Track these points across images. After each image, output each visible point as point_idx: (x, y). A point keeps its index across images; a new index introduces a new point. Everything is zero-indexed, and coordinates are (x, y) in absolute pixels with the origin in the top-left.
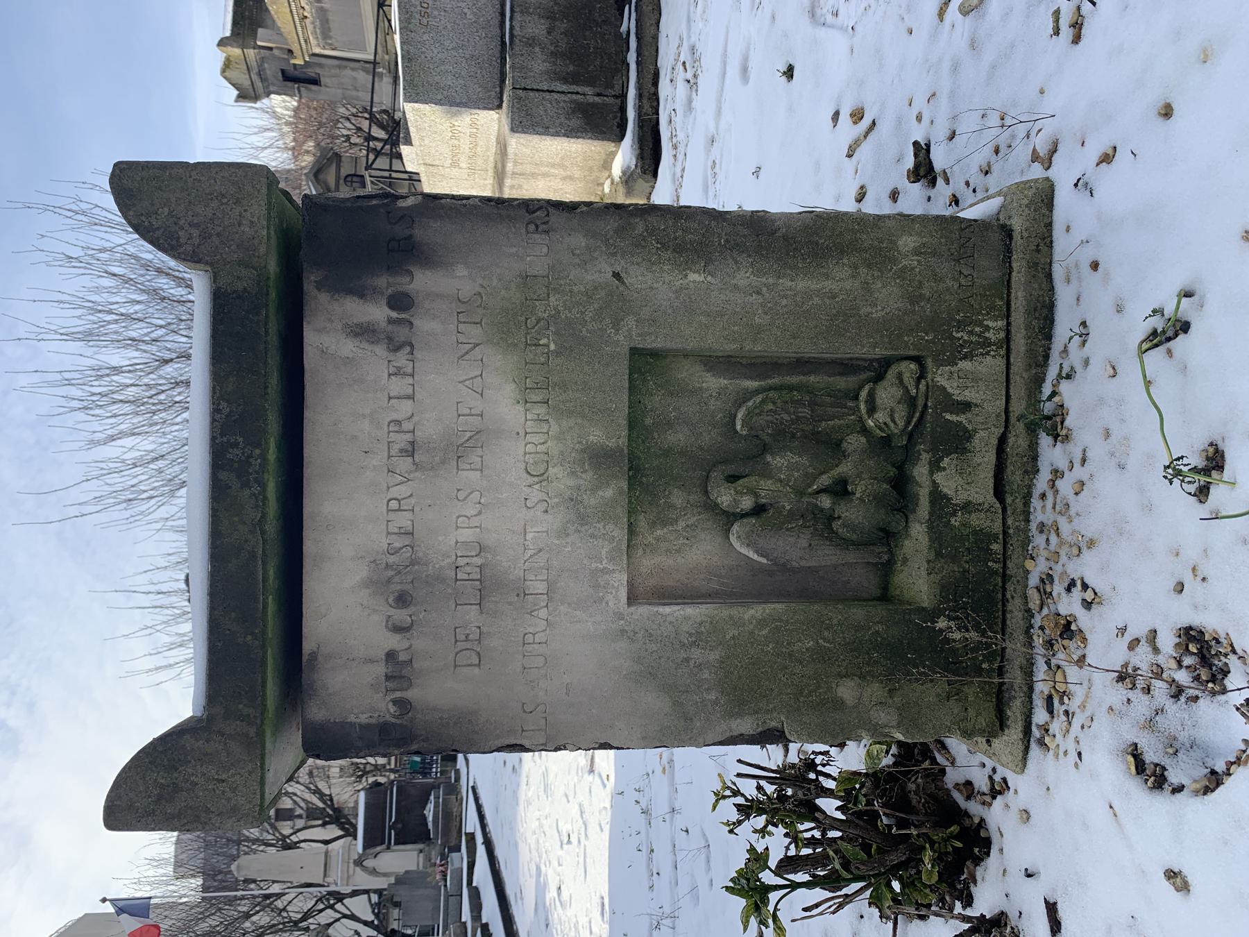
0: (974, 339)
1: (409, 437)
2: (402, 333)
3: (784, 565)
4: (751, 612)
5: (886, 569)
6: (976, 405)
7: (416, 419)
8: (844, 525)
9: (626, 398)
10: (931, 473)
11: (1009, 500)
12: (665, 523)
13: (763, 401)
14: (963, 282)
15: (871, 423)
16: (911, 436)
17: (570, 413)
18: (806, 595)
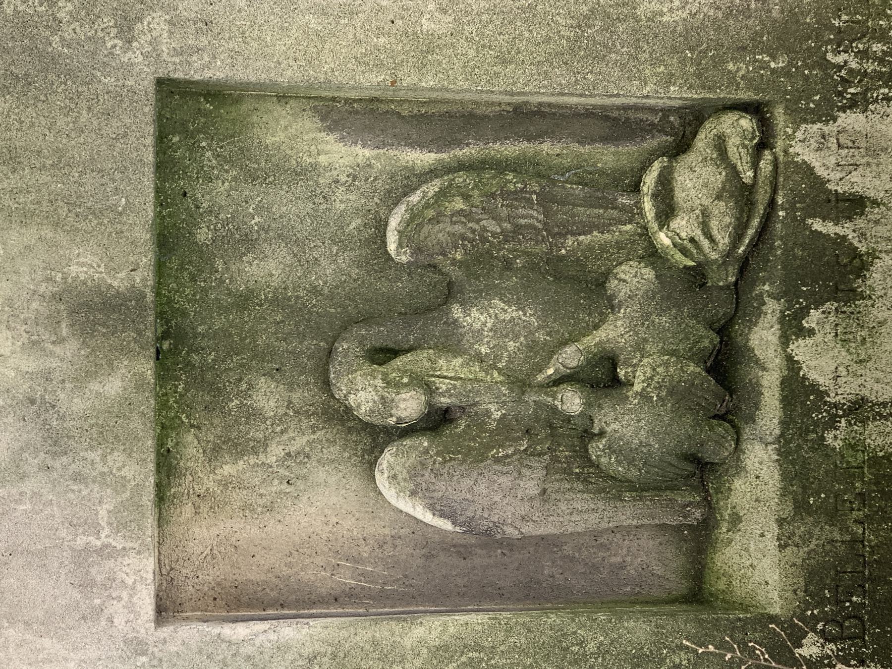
0: (871, 67)
3: (488, 533)
4: (418, 632)
5: (699, 540)
6: (875, 203)
8: (610, 449)
9: (148, 182)
10: (785, 340)
12: (239, 447)
13: (443, 194)
15: (663, 239)
16: (744, 266)
17: (26, 217)
18: (533, 594)
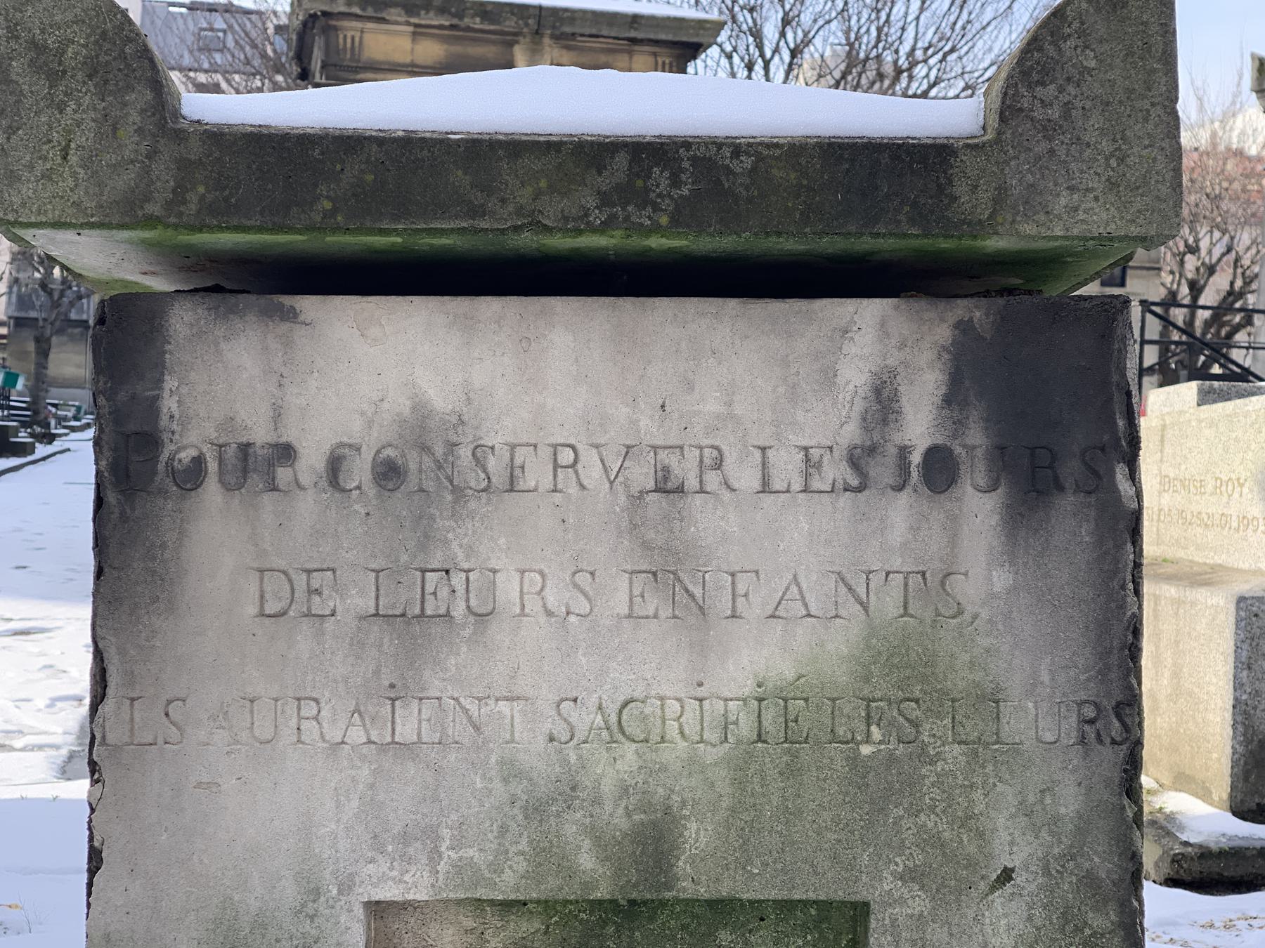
1: (692, 483)
2: (882, 471)
7: (726, 496)
17: (740, 784)
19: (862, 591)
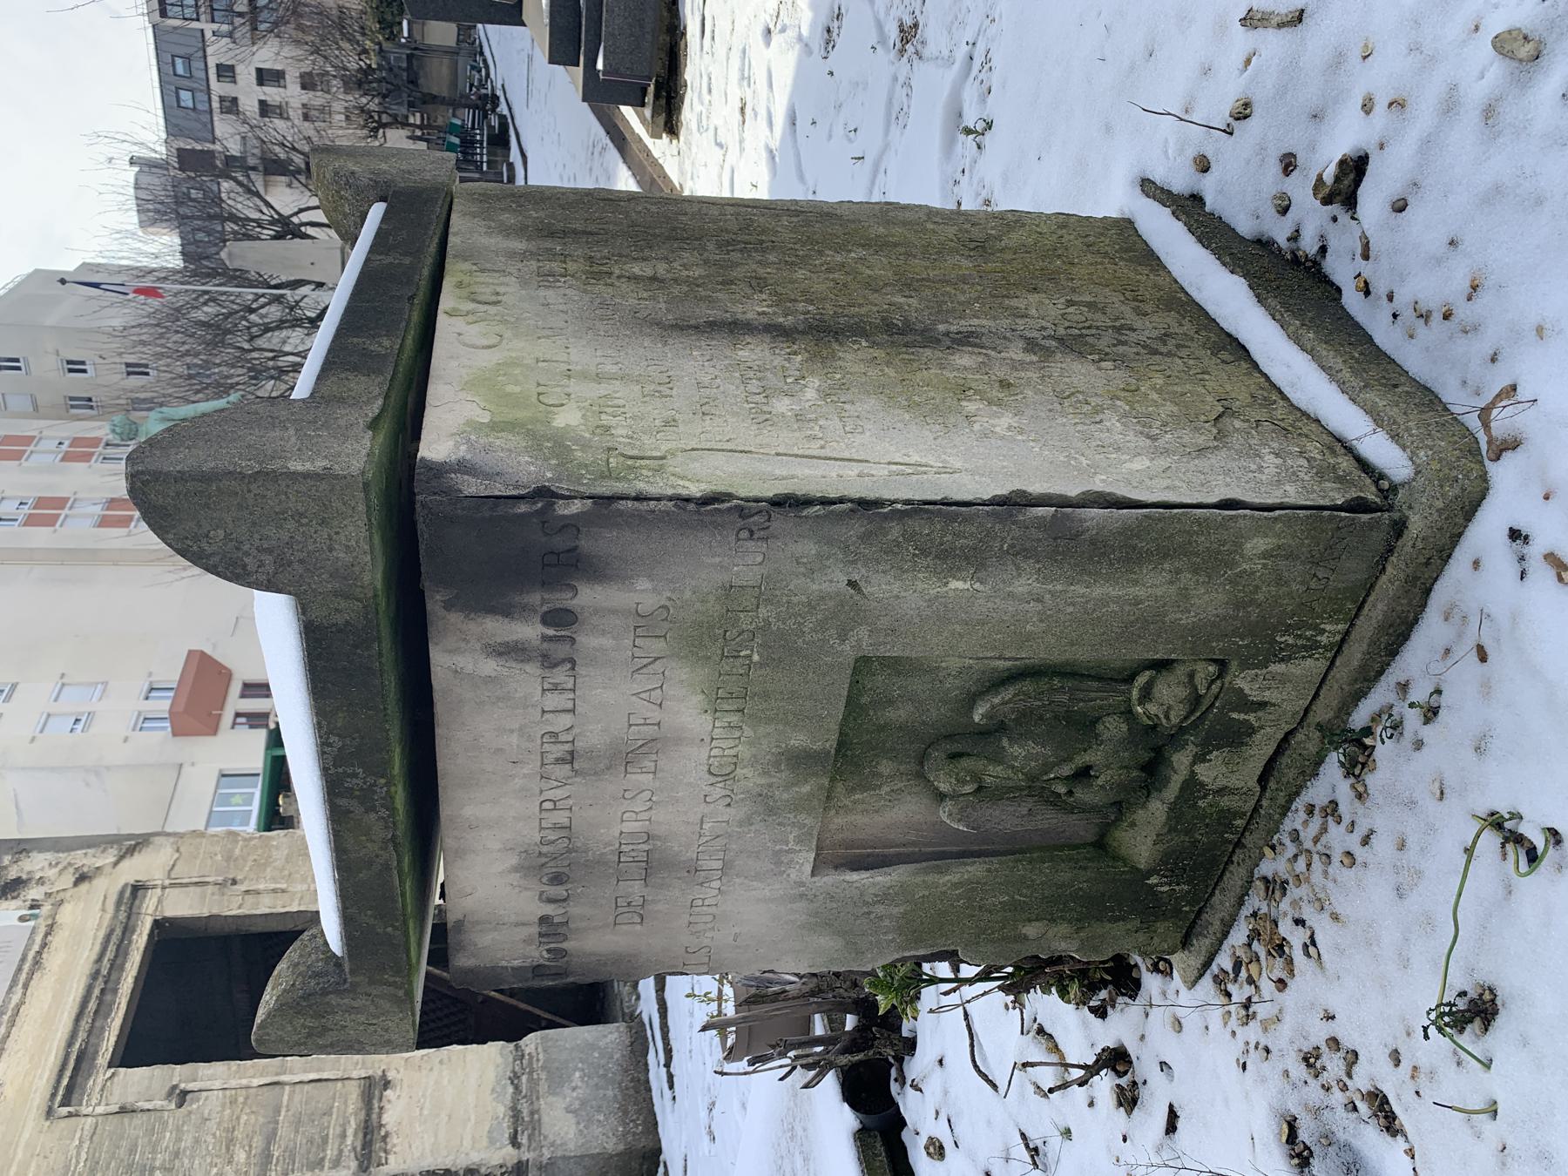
1: (568, 747)
2: (562, 650)
7: (576, 731)
10: (1194, 763)
11: (1272, 785)
12: (864, 788)
14: (1313, 585)
17: (769, 721)
19: (643, 696)
